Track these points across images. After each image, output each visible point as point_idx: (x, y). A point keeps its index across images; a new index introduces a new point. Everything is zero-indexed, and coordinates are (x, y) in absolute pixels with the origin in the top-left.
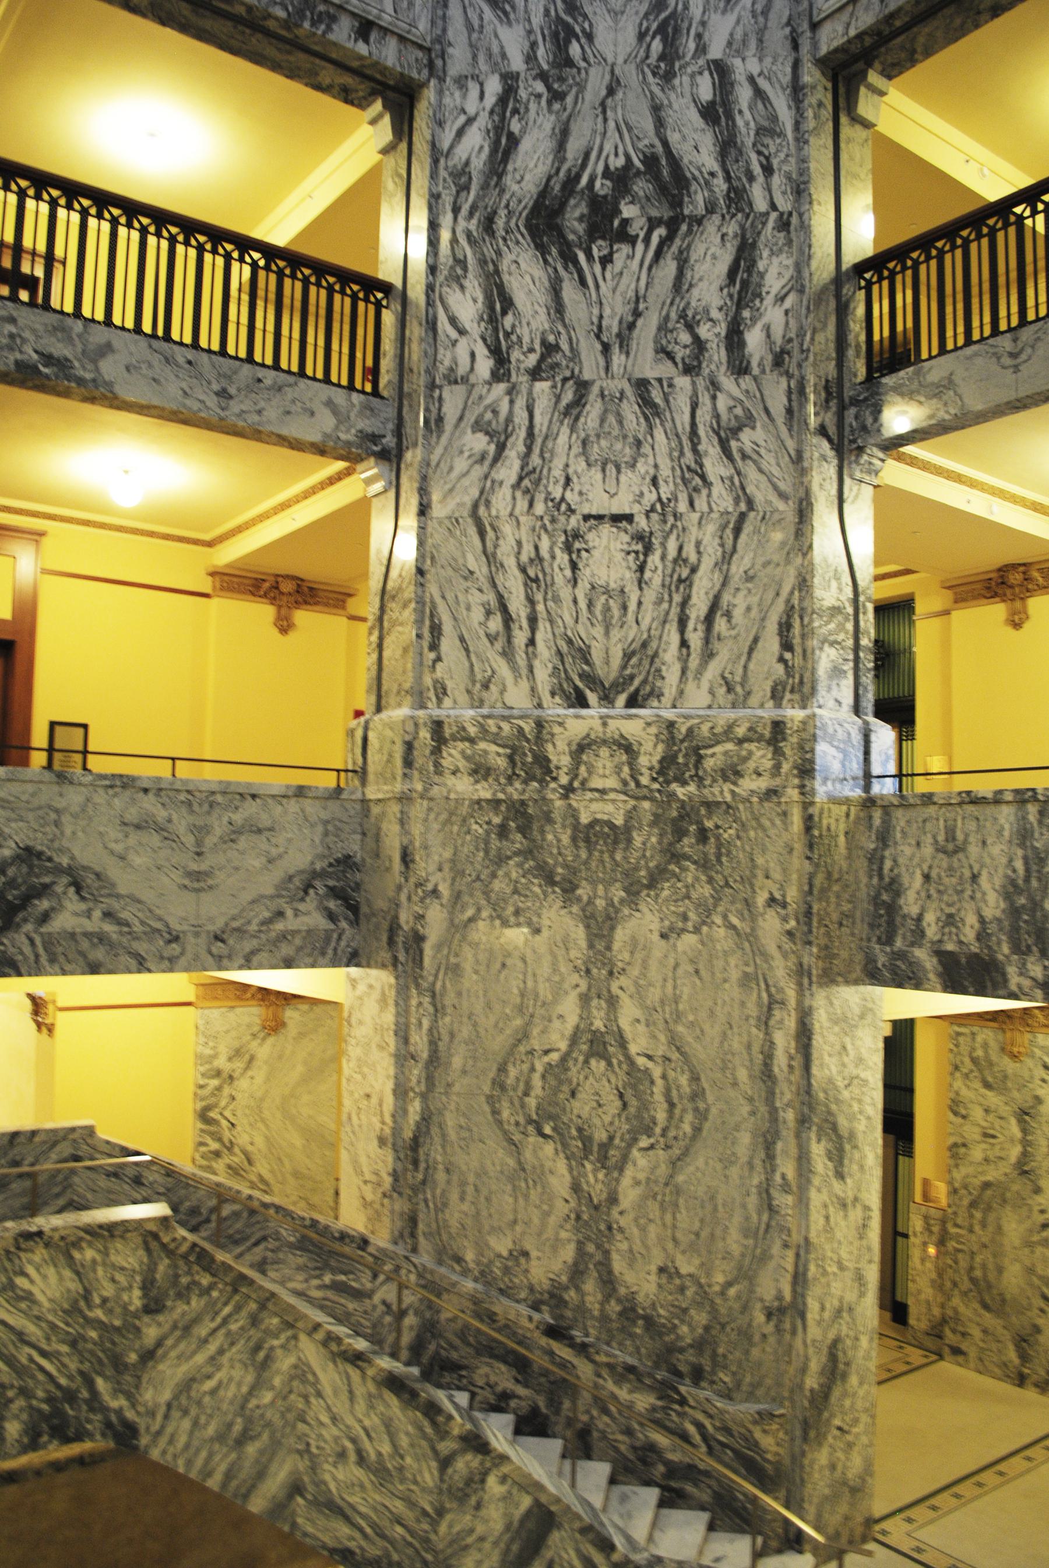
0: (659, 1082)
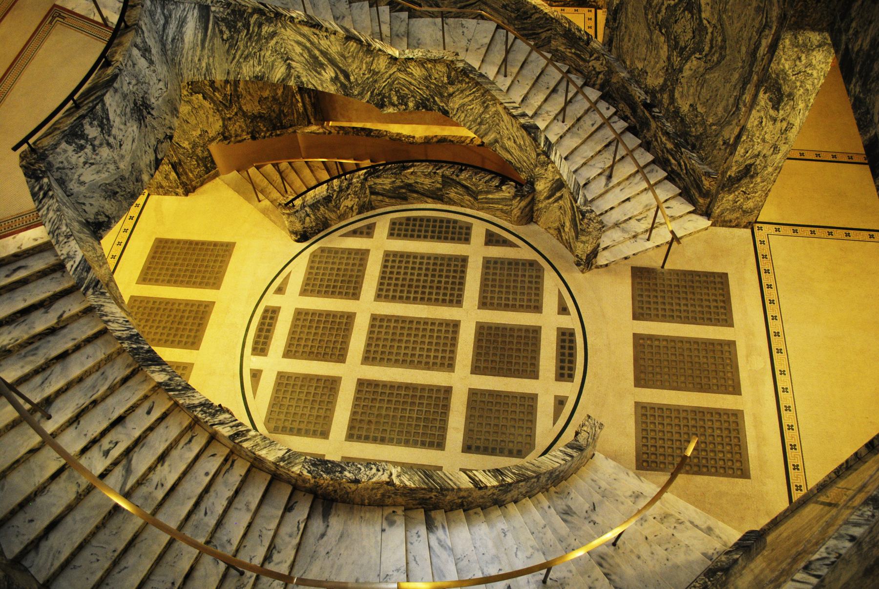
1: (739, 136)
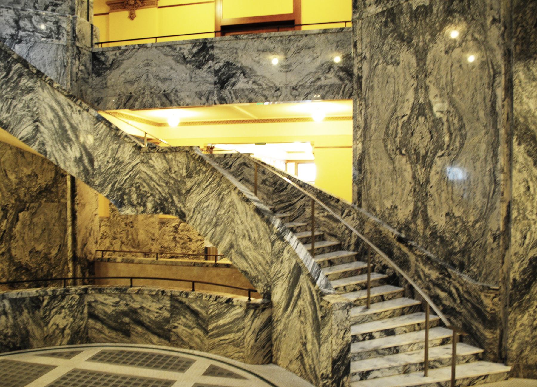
0: (446, 124)
1: (508, 219)
